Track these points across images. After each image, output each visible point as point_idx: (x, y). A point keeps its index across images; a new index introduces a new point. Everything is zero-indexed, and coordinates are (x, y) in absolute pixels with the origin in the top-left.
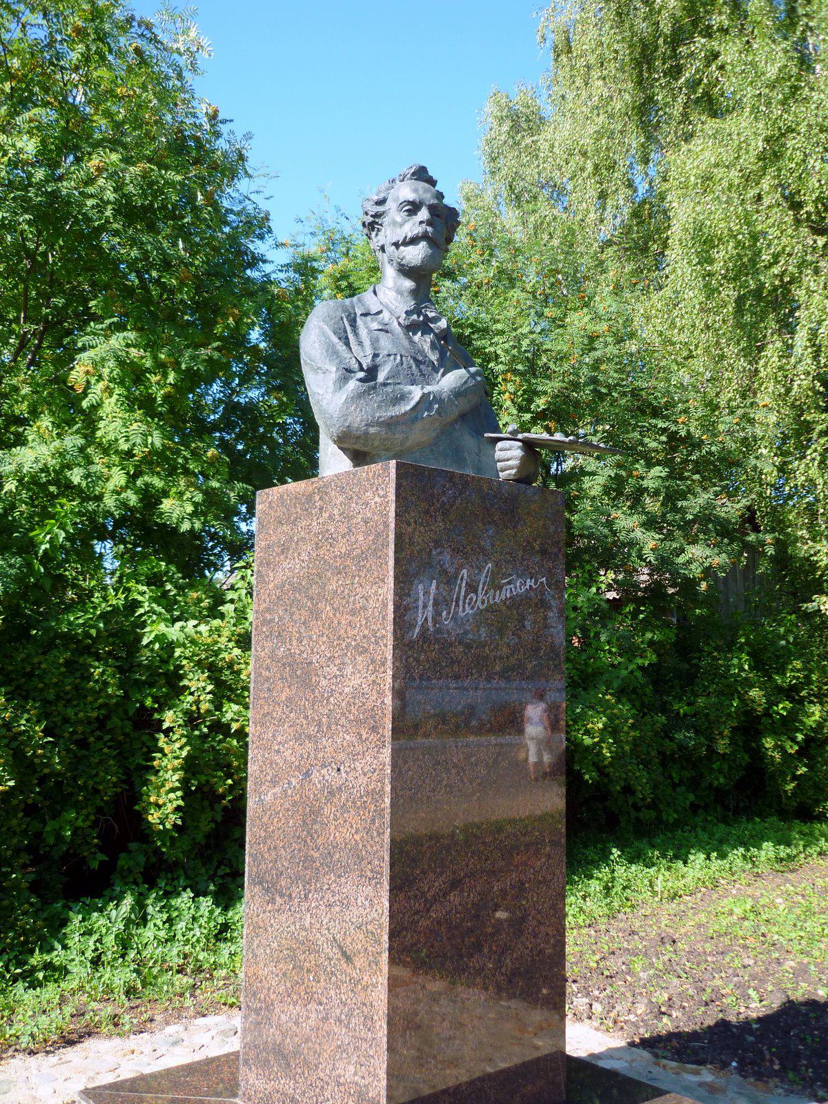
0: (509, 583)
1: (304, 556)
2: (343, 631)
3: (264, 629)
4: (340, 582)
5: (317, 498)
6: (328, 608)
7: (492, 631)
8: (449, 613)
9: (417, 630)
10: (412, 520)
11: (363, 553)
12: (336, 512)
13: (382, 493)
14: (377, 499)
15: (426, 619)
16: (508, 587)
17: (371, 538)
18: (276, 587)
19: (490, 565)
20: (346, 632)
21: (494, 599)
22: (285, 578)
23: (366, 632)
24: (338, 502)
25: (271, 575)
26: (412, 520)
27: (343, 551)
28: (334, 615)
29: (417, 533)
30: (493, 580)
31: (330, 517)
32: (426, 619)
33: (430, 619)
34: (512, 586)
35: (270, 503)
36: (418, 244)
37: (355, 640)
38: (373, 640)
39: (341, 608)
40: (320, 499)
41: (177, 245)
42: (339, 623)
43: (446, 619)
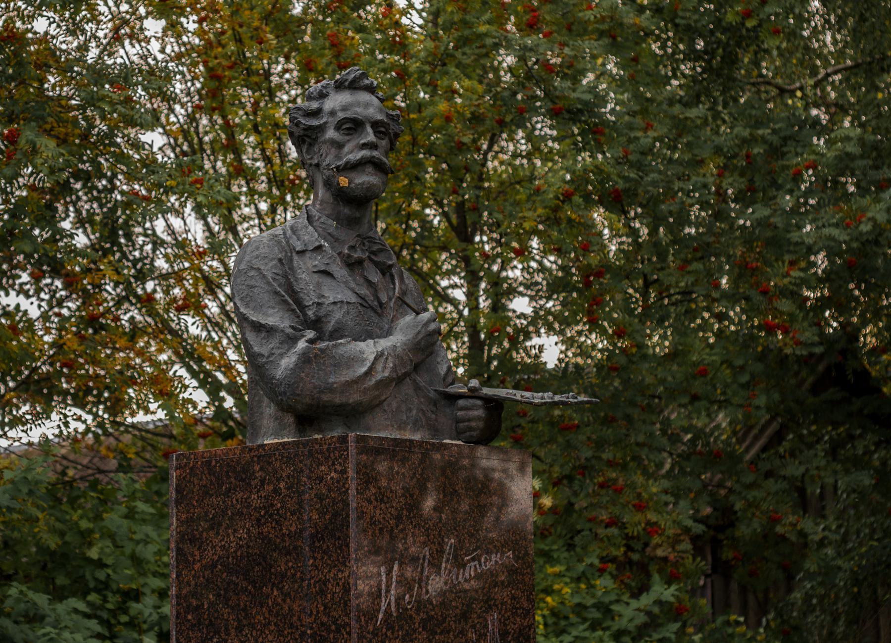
0: (473, 559)
1: (243, 534)
2: (295, 619)
3: (189, 617)
4: (290, 564)
5: (257, 468)
6: (275, 593)
7: (91, 410)
8: (411, 596)
9: (381, 616)
10: (373, 497)
11: (318, 532)
12: (282, 485)
13: (338, 468)
14: (333, 474)
15: (389, 604)
16: (472, 564)
17: (327, 517)
18: (204, 567)
19: (453, 541)
20: (299, 619)
21: (457, 578)
22: (216, 558)
23: (325, 619)
24: (284, 475)
25: (197, 553)
26: (373, 497)
27: (293, 529)
28: (284, 601)
29: (378, 512)
30: (455, 557)
31: (276, 491)
32: (389, 604)
33: (393, 605)
34: (476, 562)
35: (192, 469)
36: (347, 163)
37: (311, 628)
38: (333, 627)
39: (292, 594)
40: (261, 469)
41: (415, 429)
42: (290, 609)
43: (409, 603)
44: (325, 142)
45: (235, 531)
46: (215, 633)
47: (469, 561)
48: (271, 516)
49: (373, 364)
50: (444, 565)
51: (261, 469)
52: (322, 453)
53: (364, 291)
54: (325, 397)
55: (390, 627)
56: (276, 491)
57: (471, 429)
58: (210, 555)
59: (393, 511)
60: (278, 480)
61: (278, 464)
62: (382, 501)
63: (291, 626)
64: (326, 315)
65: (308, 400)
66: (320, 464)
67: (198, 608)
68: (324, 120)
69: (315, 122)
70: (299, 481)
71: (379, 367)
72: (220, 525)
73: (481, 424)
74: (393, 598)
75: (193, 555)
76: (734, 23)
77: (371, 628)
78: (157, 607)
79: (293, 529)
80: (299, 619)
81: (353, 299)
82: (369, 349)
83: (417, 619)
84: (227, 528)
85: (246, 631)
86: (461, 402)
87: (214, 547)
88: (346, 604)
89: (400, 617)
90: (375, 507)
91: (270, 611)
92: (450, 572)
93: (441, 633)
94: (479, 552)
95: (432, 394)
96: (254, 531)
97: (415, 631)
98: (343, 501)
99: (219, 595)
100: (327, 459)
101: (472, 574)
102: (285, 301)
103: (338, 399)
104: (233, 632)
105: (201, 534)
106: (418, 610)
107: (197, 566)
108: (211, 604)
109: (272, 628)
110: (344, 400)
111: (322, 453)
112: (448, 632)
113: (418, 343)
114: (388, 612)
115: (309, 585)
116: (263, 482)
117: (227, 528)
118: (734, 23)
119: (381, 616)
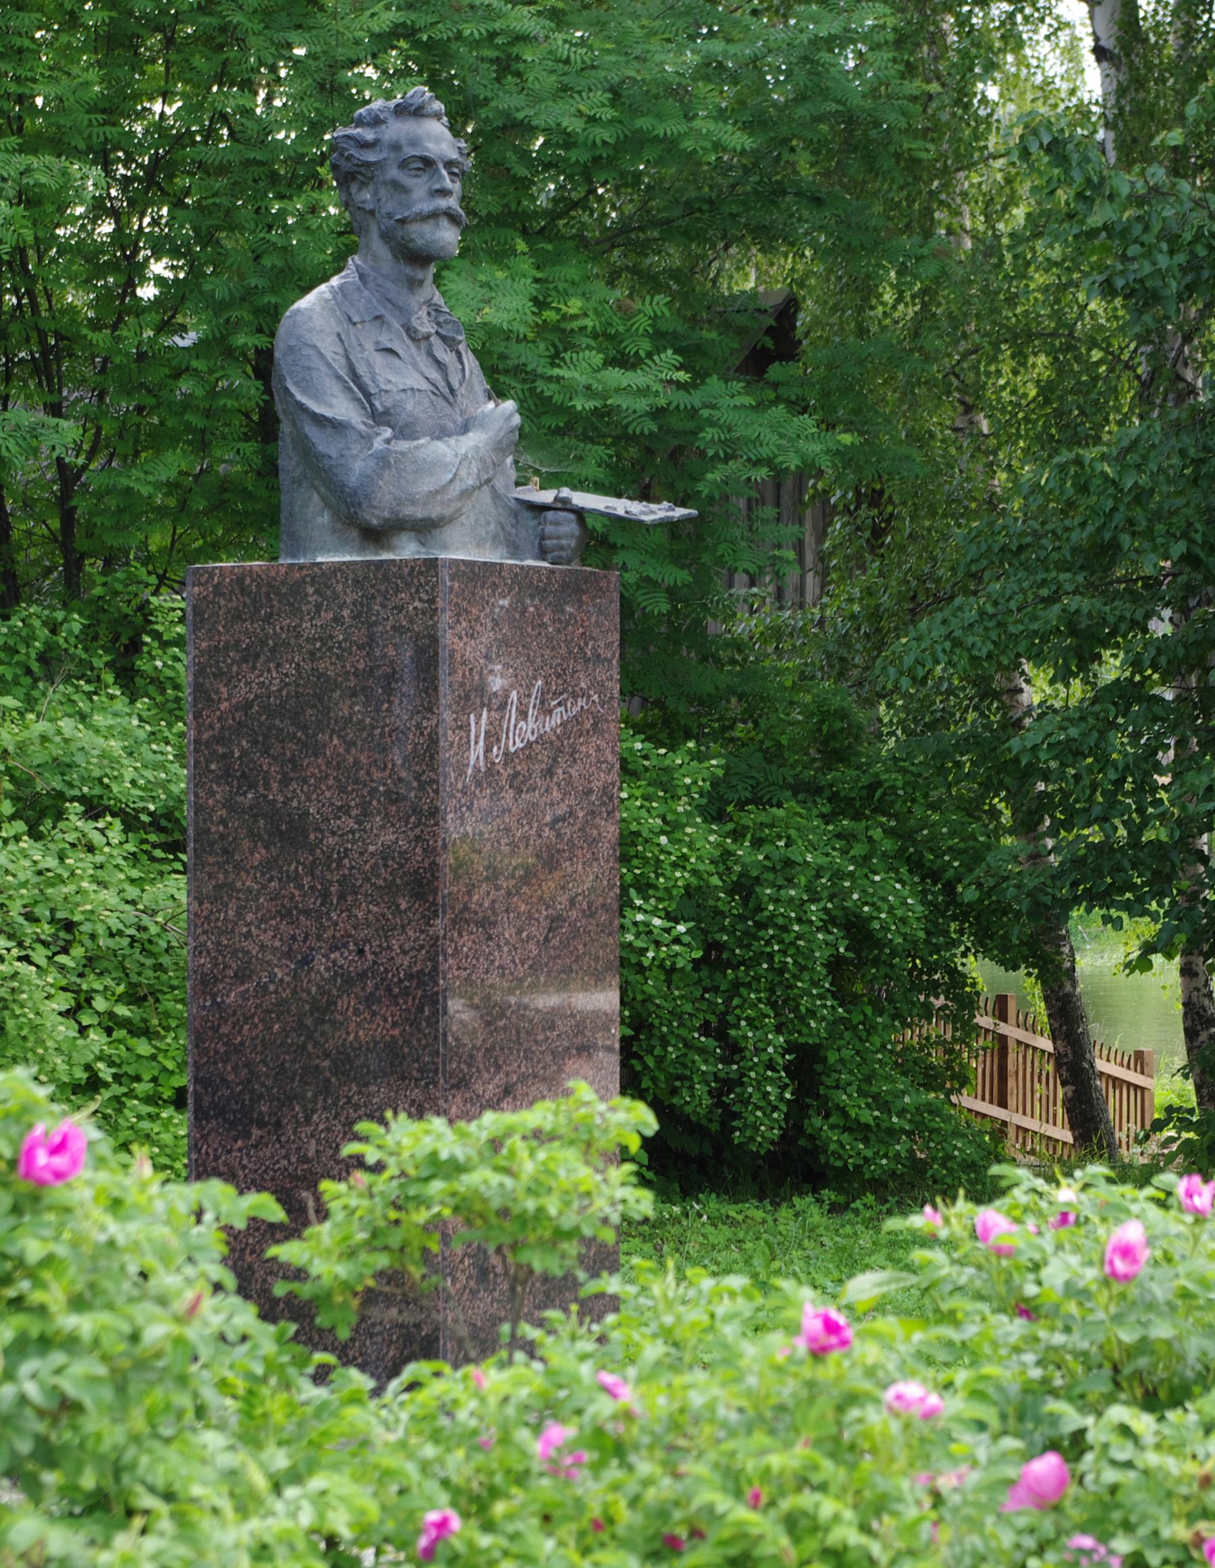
5: (310, 590)
12: (346, 613)
20: (368, 773)
25: (224, 690)
27: (361, 666)
31: (338, 620)
35: (217, 586)
40: (317, 592)
44: (385, 183)
45: (279, 665)
46: (250, 787)
48: (330, 649)
51: (317, 592)
52: (401, 577)
53: (435, 375)
55: (479, 784)
56: (338, 620)
57: (562, 548)
58: (242, 692)
60: (341, 607)
61: (340, 588)
63: (356, 782)
65: (386, 514)
66: (397, 591)
67: (224, 756)
68: (384, 155)
69: (371, 157)
70: (370, 609)
72: (257, 656)
73: (573, 543)
75: (217, 692)
76: (938, 1200)
79: (361, 666)
80: (368, 773)
81: (424, 385)
82: (445, 449)
84: (268, 661)
85: (294, 785)
86: (550, 515)
87: (247, 684)
88: (432, 757)
91: (328, 764)
95: (513, 504)
96: (307, 667)
98: (430, 637)
99: (255, 742)
100: (408, 585)
102: (349, 389)
104: (275, 786)
105: (230, 667)
107: (224, 706)
108: (244, 753)
109: (331, 782)
111: (401, 577)
115: (382, 735)
116: (318, 608)
117: (268, 661)
118: (938, 1200)
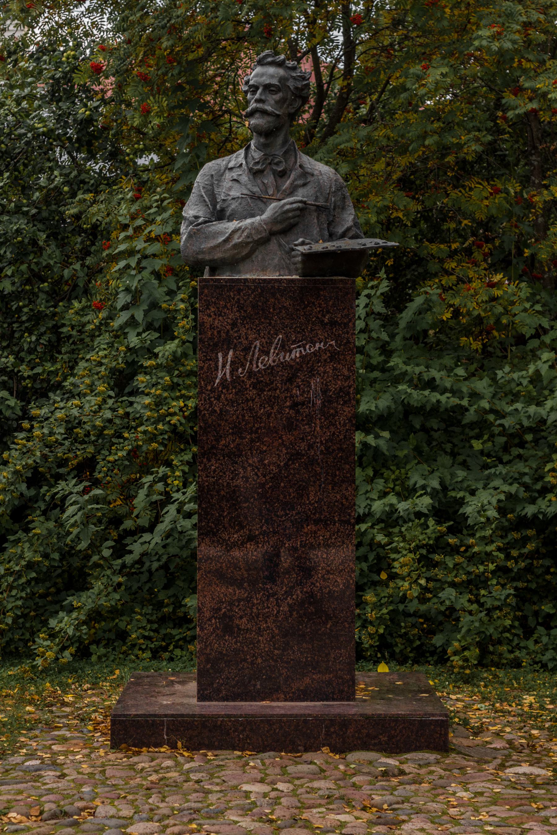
0: (299, 347)
9: (217, 381)
16: (298, 350)
21: (284, 358)
32: (225, 374)
33: (228, 376)
34: (302, 349)
47: (295, 348)
49: (230, 235)
50: (272, 351)
54: (200, 257)
59: (229, 321)
62: (220, 315)
64: (227, 207)
71: (236, 236)
74: (228, 371)
77: (209, 388)
78: (455, 445)
83: (248, 383)
89: (233, 381)
90: (214, 319)
92: (278, 354)
93: (269, 391)
94: (304, 342)
97: (246, 389)
101: (298, 355)
102: (205, 201)
103: (207, 257)
106: (249, 377)
110: (211, 257)
112: (276, 390)
113: (275, 219)
114: (224, 379)
119: (217, 381)
